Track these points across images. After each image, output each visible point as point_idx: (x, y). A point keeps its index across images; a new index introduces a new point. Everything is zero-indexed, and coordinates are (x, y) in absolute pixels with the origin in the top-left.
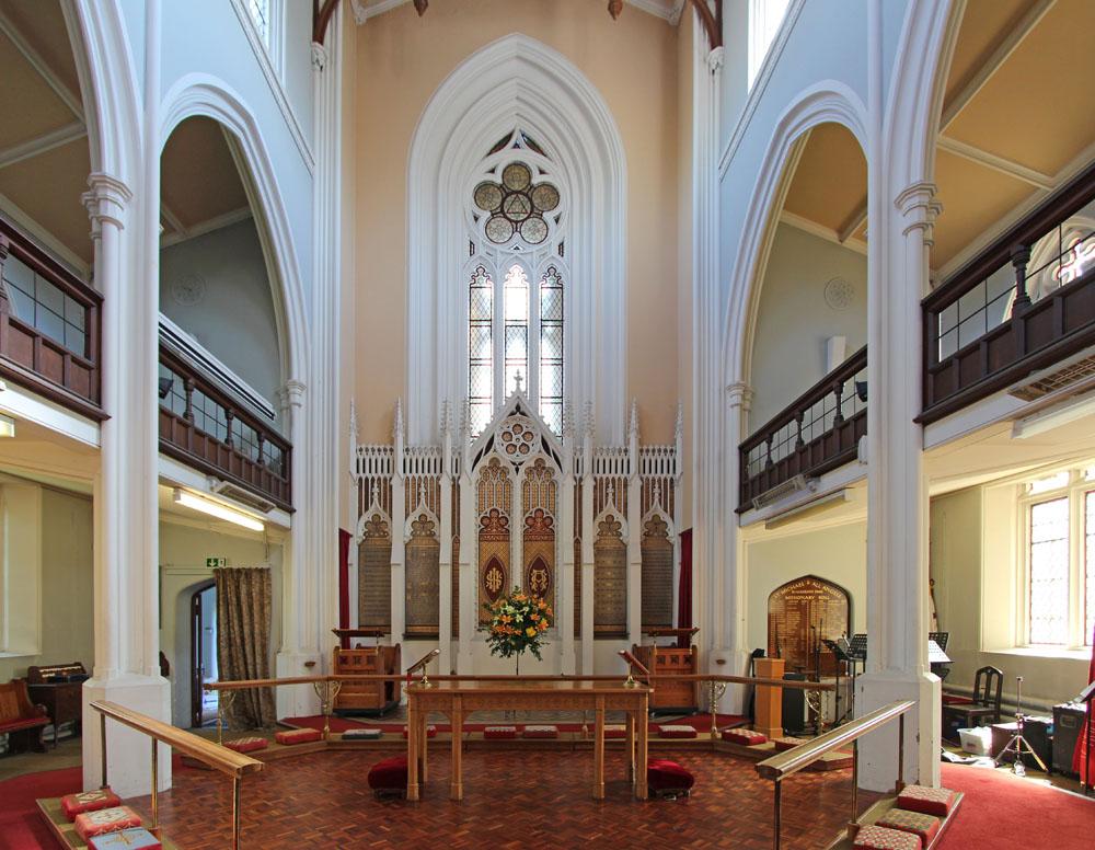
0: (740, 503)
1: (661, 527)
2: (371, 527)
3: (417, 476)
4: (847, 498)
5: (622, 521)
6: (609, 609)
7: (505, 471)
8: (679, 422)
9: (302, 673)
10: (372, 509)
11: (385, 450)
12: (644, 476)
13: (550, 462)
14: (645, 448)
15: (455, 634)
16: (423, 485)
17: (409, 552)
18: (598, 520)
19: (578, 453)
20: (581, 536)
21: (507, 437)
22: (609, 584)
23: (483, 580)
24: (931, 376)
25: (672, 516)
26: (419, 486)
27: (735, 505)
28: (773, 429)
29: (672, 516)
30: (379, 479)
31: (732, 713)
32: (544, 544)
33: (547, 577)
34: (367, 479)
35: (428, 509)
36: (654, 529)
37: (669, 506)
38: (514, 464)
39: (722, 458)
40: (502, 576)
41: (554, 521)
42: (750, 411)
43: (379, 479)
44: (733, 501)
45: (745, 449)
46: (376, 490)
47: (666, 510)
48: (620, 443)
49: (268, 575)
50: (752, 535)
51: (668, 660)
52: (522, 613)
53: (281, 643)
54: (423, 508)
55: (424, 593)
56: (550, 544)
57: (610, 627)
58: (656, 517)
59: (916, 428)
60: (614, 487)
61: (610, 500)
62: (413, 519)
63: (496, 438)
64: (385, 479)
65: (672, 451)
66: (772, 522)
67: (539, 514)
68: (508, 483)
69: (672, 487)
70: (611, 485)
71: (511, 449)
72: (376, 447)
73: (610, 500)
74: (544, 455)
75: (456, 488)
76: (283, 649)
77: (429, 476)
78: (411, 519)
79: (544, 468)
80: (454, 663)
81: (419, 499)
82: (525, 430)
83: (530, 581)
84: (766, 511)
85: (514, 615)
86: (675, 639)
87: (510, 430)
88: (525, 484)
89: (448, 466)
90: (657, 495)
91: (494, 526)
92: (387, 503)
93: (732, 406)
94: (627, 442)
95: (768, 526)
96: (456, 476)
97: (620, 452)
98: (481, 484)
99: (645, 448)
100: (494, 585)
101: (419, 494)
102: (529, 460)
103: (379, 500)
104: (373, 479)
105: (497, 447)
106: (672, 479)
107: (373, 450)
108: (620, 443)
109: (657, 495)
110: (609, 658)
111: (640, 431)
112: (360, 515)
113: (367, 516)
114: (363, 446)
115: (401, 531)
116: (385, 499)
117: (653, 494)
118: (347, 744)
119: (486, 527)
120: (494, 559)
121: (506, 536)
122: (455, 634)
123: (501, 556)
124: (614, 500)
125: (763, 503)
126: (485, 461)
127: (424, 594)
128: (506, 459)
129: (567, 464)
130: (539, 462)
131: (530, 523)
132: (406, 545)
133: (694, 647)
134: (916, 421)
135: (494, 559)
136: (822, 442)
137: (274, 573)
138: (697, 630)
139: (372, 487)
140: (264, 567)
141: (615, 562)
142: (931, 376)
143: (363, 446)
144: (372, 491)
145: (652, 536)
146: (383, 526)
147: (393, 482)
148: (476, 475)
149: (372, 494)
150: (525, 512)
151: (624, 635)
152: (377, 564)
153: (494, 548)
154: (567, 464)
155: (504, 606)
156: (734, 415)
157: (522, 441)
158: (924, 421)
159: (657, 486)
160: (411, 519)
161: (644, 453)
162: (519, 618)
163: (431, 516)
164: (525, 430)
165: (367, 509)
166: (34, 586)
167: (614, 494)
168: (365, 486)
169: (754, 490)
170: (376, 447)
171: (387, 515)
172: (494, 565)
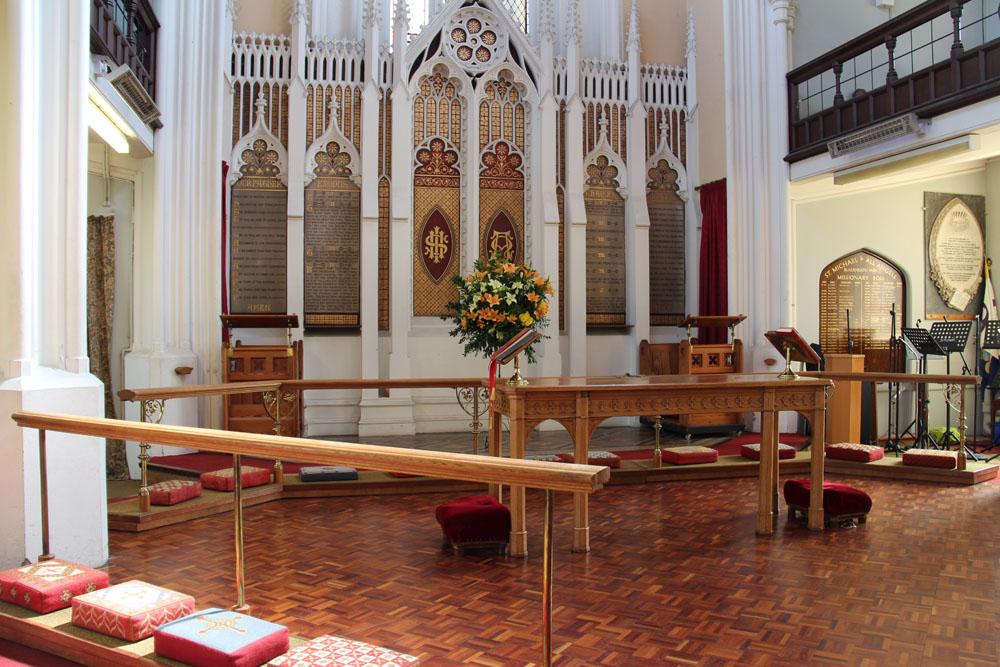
0: (791, 149)
1: (669, 176)
2: (324, 159)
3: (325, 84)
4: (972, 145)
5: (619, 164)
6: (602, 290)
7: (452, 85)
8: (691, 37)
9: (170, 382)
10: (255, 132)
11: (277, 43)
12: (587, 101)
13: (520, 76)
14: (647, 67)
15: (384, 326)
16: (334, 97)
17: (310, 197)
18: (589, 162)
19: (587, 69)
20: (390, 175)
21: (459, 36)
22: (602, 255)
23: (421, 245)
24: (794, 129)
25: (684, 162)
26: (329, 100)
27: (784, 152)
28: (845, 55)
29: (684, 162)
30: (267, 86)
31: (789, 432)
32: (508, 193)
33: (514, 242)
34: (247, 85)
35: (342, 134)
36: (661, 181)
37: (680, 148)
38: (470, 75)
39: (763, 87)
40: (449, 239)
41: (460, 160)
42: (793, 31)
43: (267, 86)
44: (780, 144)
45: (794, 79)
46: (262, 102)
47: (676, 154)
48: (614, 57)
49: (111, 227)
50: (815, 187)
51: (706, 360)
52: (513, 292)
53: (130, 337)
54: (260, 128)
55: (338, 262)
56: (517, 194)
57: (608, 319)
58: (663, 162)
59: (785, 164)
60: (608, 118)
61: (603, 135)
62: (318, 149)
63: (444, 39)
64: (276, 87)
65: (681, 75)
66: (842, 177)
67: (437, 147)
68: (458, 103)
69: (683, 123)
70: (604, 114)
71: (465, 54)
72: (263, 38)
73: (603, 135)
74: (512, 65)
75: (386, 106)
76: (136, 346)
77: (334, 85)
78: (242, 145)
79: (445, 79)
80: (384, 365)
81: (328, 119)
82: (484, 28)
83: (490, 248)
84: (843, 160)
85: (503, 294)
86: (694, 332)
87: (464, 26)
88: (483, 104)
89: (374, 71)
90: (664, 132)
91: (437, 164)
92: (280, 123)
93: (776, 23)
94: (625, 57)
95: (837, 181)
96: (385, 87)
97: (615, 69)
98: (419, 100)
99: (647, 67)
100: (437, 254)
101: (328, 111)
102: (491, 71)
103: (267, 117)
104: (257, 86)
105: (446, 48)
106: (682, 113)
107: (258, 42)
108: (614, 57)
109: (664, 132)
110: (617, 360)
111: (642, 43)
112: (236, 139)
113: (246, 142)
114: (244, 36)
115: (299, 167)
116: (276, 117)
117: (599, 127)
118: (314, 488)
119: (426, 164)
120: (437, 211)
121: (454, 178)
122: (384, 326)
123: (447, 209)
124: (608, 135)
125: (843, 149)
126: (426, 68)
127: (332, 265)
128: (457, 67)
129: (545, 81)
130: (505, 75)
131: (490, 162)
132: (306, 188)
133: (738, 342)
134: (785, 160)
135: (437, 211)
136: (932, 74)
137: (119, 227)
138: (737, 320)
139: (256, 97)
140: (105, 215)
141: (609, 223)
142: (794, 129)
143: (244, 36)
144: (256, 102)
145: (657, 188)
146: (342, 160)
147: (291, 92)
148: (414, 87)
149: (256, 108)
150: (482, 145)
151: (622, 328)
152: (261, 216)
153: (439, 197)
154: (545, 81)
155: (486, 279)
156: (778, 36)
157: (480, 43)
158: (791, 160)
159: (664, 119)
160: (242, 145)
161: (647, 74)
162: (511, 299)
163: (347, 146)
164: (484, 28)
165: (246, 130)
166: (630, 267)
167: (608, 127)
168: (245, 99)
169: (809, 137)
170: (263, 38)
171: (278, 141)
172: (436, 222)
